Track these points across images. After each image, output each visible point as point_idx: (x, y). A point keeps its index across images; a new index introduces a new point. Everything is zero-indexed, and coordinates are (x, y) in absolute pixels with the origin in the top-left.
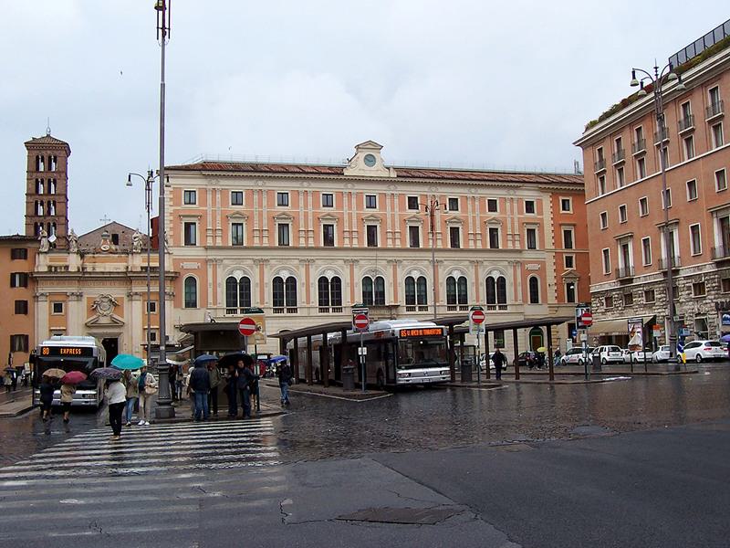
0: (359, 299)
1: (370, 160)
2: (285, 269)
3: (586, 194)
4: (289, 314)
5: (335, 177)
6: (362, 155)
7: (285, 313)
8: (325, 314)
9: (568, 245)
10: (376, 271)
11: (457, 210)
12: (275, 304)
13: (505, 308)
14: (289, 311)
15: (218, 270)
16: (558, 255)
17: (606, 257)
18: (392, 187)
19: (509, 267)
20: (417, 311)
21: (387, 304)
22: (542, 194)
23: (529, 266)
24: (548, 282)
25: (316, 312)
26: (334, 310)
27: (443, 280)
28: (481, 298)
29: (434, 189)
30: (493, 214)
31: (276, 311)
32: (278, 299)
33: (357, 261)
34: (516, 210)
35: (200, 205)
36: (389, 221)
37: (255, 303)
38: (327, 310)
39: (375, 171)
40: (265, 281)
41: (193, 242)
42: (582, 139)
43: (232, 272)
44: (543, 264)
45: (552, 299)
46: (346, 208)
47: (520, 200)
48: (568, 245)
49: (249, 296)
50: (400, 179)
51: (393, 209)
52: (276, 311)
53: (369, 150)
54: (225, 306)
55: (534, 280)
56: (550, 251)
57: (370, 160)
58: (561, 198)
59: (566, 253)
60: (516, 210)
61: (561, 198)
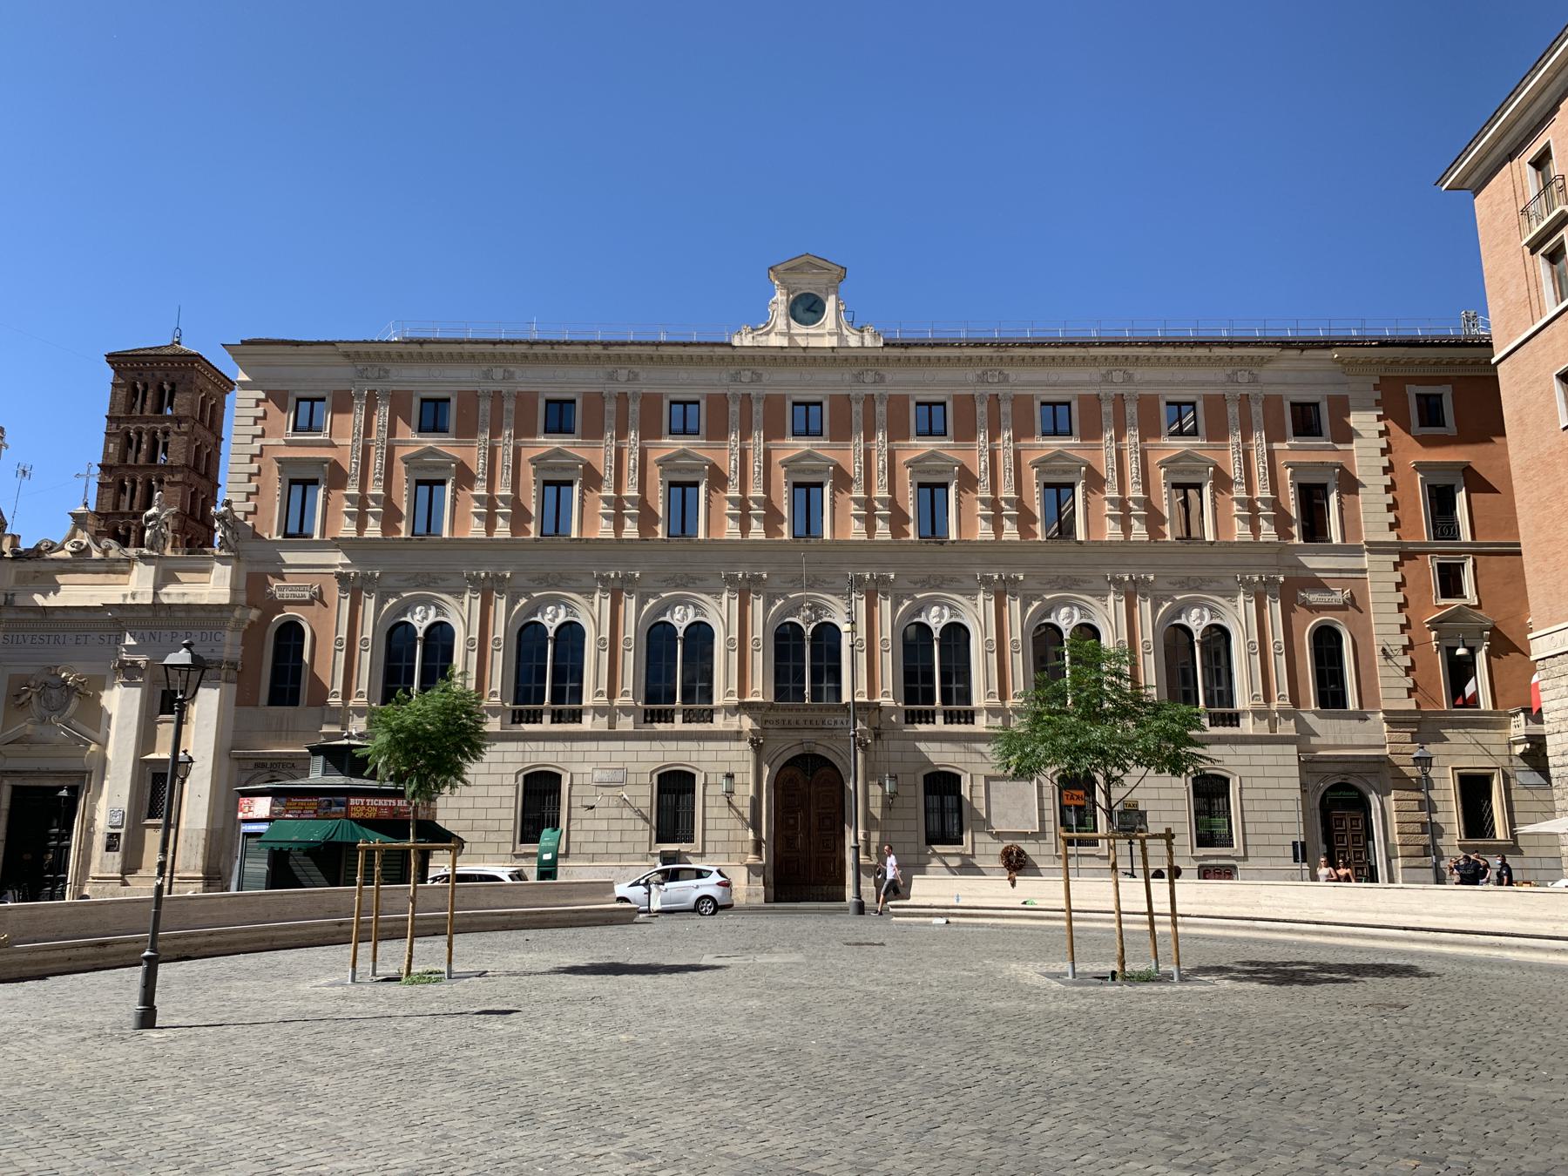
0: (760, 690)
45: (1393, 692)
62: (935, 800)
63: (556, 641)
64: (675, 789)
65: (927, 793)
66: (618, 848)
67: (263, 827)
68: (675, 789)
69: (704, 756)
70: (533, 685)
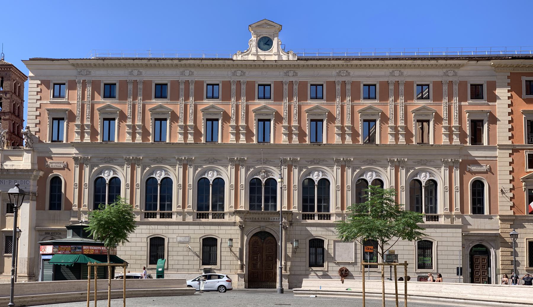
0: (243, 205)
49: (327, 199)
62: (313, 250)
64: (209, 245)
65: (310, 247)
66: (187, 267)
67: (50, 257)
68: (209, 245)
69: (221, 232)
70: (152, 203)
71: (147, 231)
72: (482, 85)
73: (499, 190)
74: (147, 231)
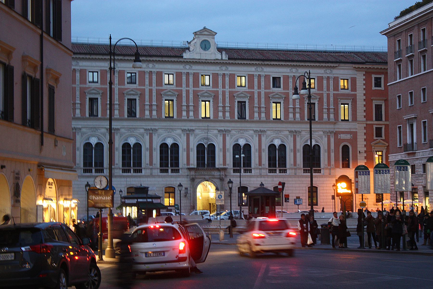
0: (194, 162)
1: (205, 46)
2: (131, 136)
3: (389, 75)
4: (135, 174)
5: (176, 59)
6: (198, 41)
7: (132, 173)
8: (89, 174)
9: (379, 118)
10: (207, 139)
11: (280, 87)
12: (270, 165)
13: (140, 171)
14: (135, 171)
15: (227, 138)
16: (368, 127)
17: (425, 127)
18: (224, 68)
19: (219, 135)
20: (94, 173)
21: (217, 166)
22: (356, 72)
23: (342, 136)
24: (359, 149)
25: (157, 172)
26: (280, 172)
27: (265, 147)
28: (191, 162)
29: (259, 69)
30: (276, 90)
31: (124, 171)
32: (126, 161)
33: (193, 130)
34: (331, 87)
35: (352, 91)
36: (220, 97)
37: (219, 162)
38: (167, 171)
39: (212, 54)
40: (191, 147)
41: (95, 113)
42: (388, 29)
43: (164, 139)
44: (355, 134)
46: (184, 85)
47: (267, 77)
48: (379, 118)
49: (177, 158)
50: (231, 62)
51: (188, 85)
52: (124, 171)
53: (205, 36)
54: (159, 166)
55: (345, 149)
56: (361, 122)
57: (205, 46)
58: (373, 76)
59: (375, 124)
60: (331, 87)
61: (373, 76)
63: (278, 150)
71: (125, 183)
72: (280, 78)
73: (358, 152)
74: (125, 183)
